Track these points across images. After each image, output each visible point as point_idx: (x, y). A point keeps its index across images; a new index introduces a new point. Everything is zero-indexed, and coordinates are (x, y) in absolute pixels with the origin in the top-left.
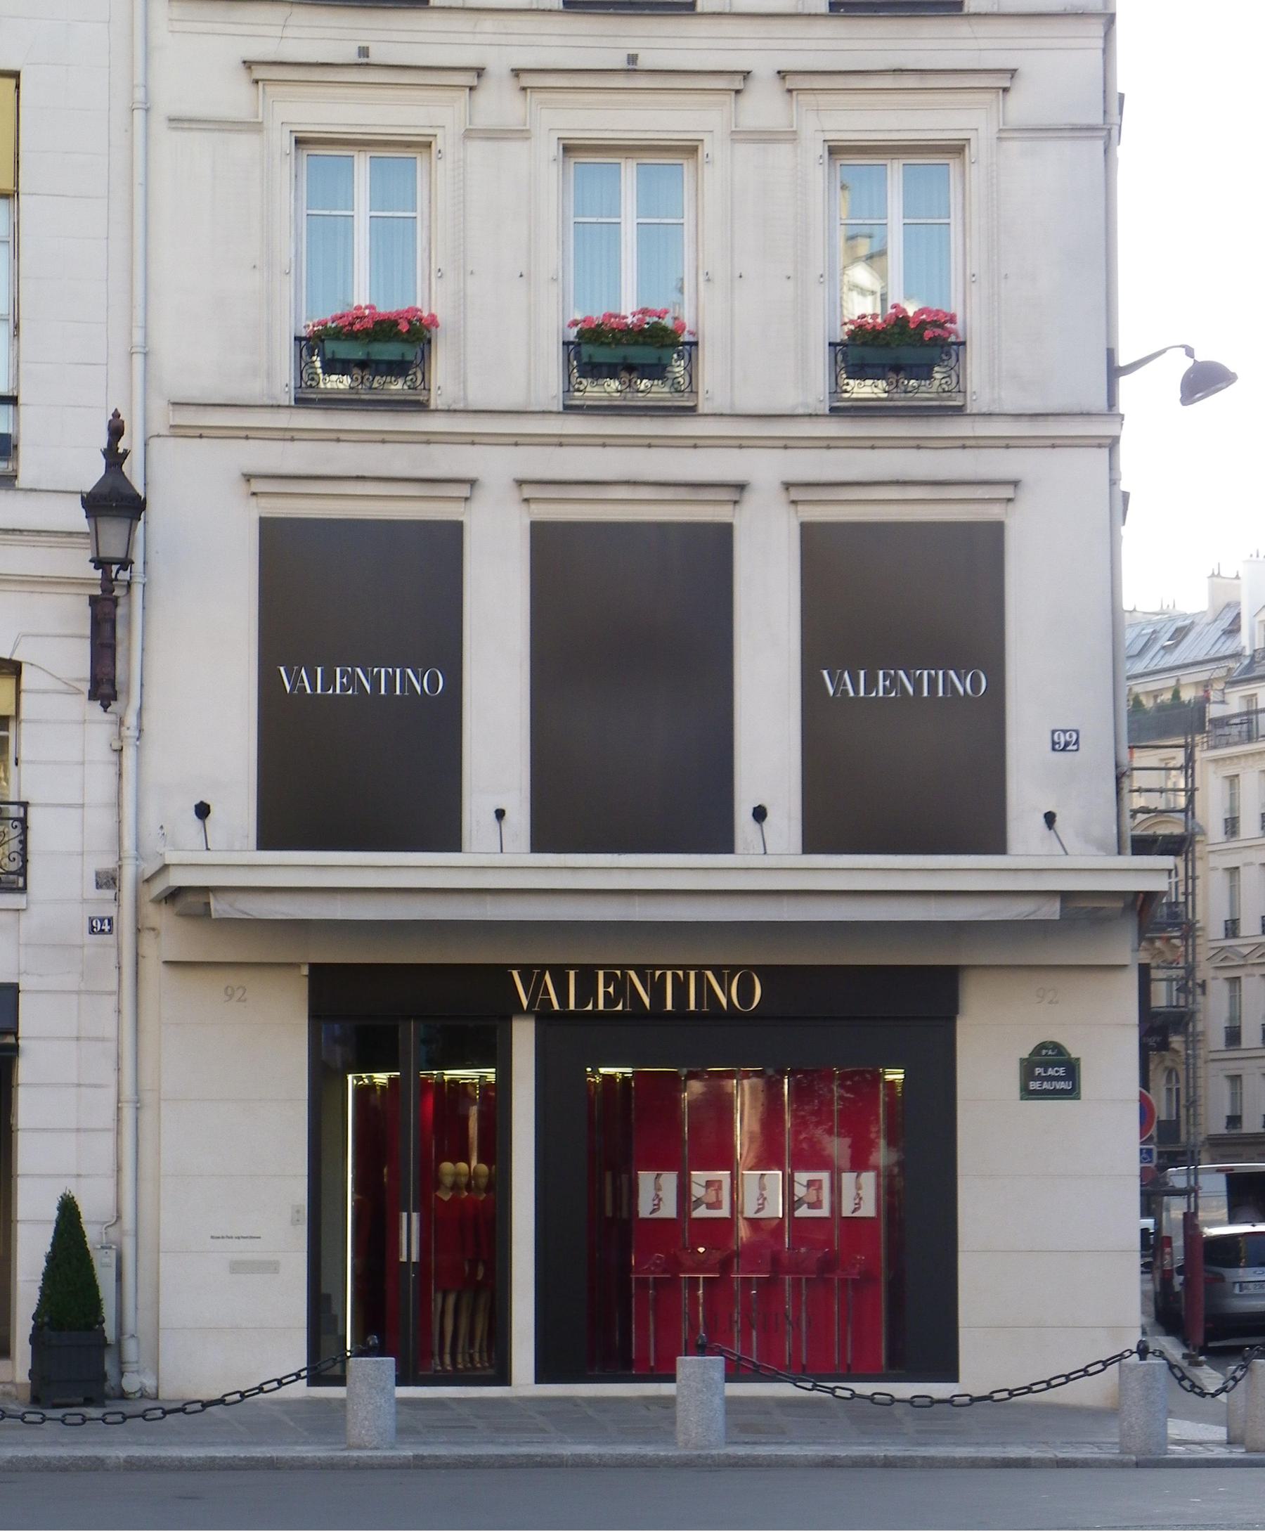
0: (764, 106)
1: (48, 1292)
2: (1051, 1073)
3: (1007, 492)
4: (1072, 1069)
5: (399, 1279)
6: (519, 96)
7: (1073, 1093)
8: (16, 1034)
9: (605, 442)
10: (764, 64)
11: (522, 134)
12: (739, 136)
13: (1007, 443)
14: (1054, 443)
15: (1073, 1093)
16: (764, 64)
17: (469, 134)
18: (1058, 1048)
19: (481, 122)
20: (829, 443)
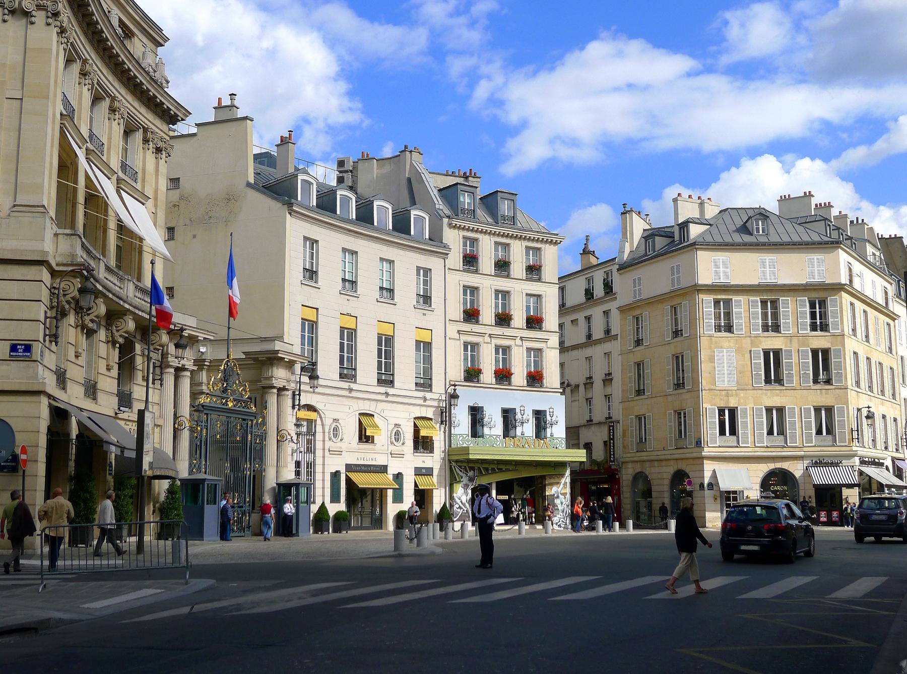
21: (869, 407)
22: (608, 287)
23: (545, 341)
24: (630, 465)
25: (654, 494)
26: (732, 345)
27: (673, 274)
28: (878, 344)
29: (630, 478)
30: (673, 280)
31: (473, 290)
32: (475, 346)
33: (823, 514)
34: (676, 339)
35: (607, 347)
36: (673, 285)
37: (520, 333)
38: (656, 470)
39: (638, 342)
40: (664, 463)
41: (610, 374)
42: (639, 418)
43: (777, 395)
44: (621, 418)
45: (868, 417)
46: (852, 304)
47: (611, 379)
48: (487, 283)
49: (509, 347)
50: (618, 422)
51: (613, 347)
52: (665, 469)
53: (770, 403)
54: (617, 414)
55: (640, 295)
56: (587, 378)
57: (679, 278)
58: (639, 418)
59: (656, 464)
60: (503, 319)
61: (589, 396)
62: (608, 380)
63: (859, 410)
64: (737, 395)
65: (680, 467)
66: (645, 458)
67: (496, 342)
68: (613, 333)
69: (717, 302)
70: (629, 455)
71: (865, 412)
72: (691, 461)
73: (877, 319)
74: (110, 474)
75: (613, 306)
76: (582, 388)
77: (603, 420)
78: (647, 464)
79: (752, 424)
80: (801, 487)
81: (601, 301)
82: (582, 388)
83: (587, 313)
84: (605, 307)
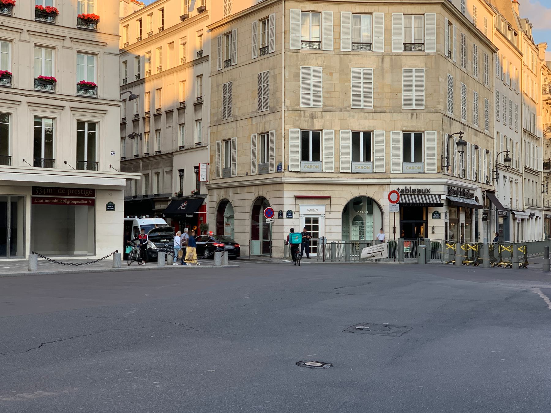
0: (68, 43)
1: (265, 201)
2: (111, 207)
3: (64, 38)
4: (114, 206)
5: (549, 169)
6: (28, 35)
7: (114, 210)
8: (342, 236)
9: (41, 97)
10: (68, 36)
11: (28, 42)
12: (64, 47)
13: (104, 104)
14: (111, 105)
15: (114, 210)
16: (68, 36)
17: (20, 41)
18: (112, 203)
19: (22, 39)
20: (77, 101)
21: (507, 152)
26: (320, 63)
28: (475, 72)
29: (215, 205)
38: (237, 197)
39: (228, 62)
40: (246, 189)
41: (201, 97)
42: (227, 141)
43: (365, 118)
45: (459, 144)
46: (463, 38)
52: (247, 196)
53: (356, 128)
56: (181, 103)
58: (227, 141)
59: (239, 190)
61: (182, 122)
62: (198, 104)
63: (450, 136)
64: (322, 117)
70: (214, 182)
71: (456, 138)
72: (271, 187)
73: (475, 48)
74: (201, 264)
76: (176, 113)
78: (231, 191)
79: (337, 148)
81: (195, 21)
82: (176, 113)
83: (183, 34)
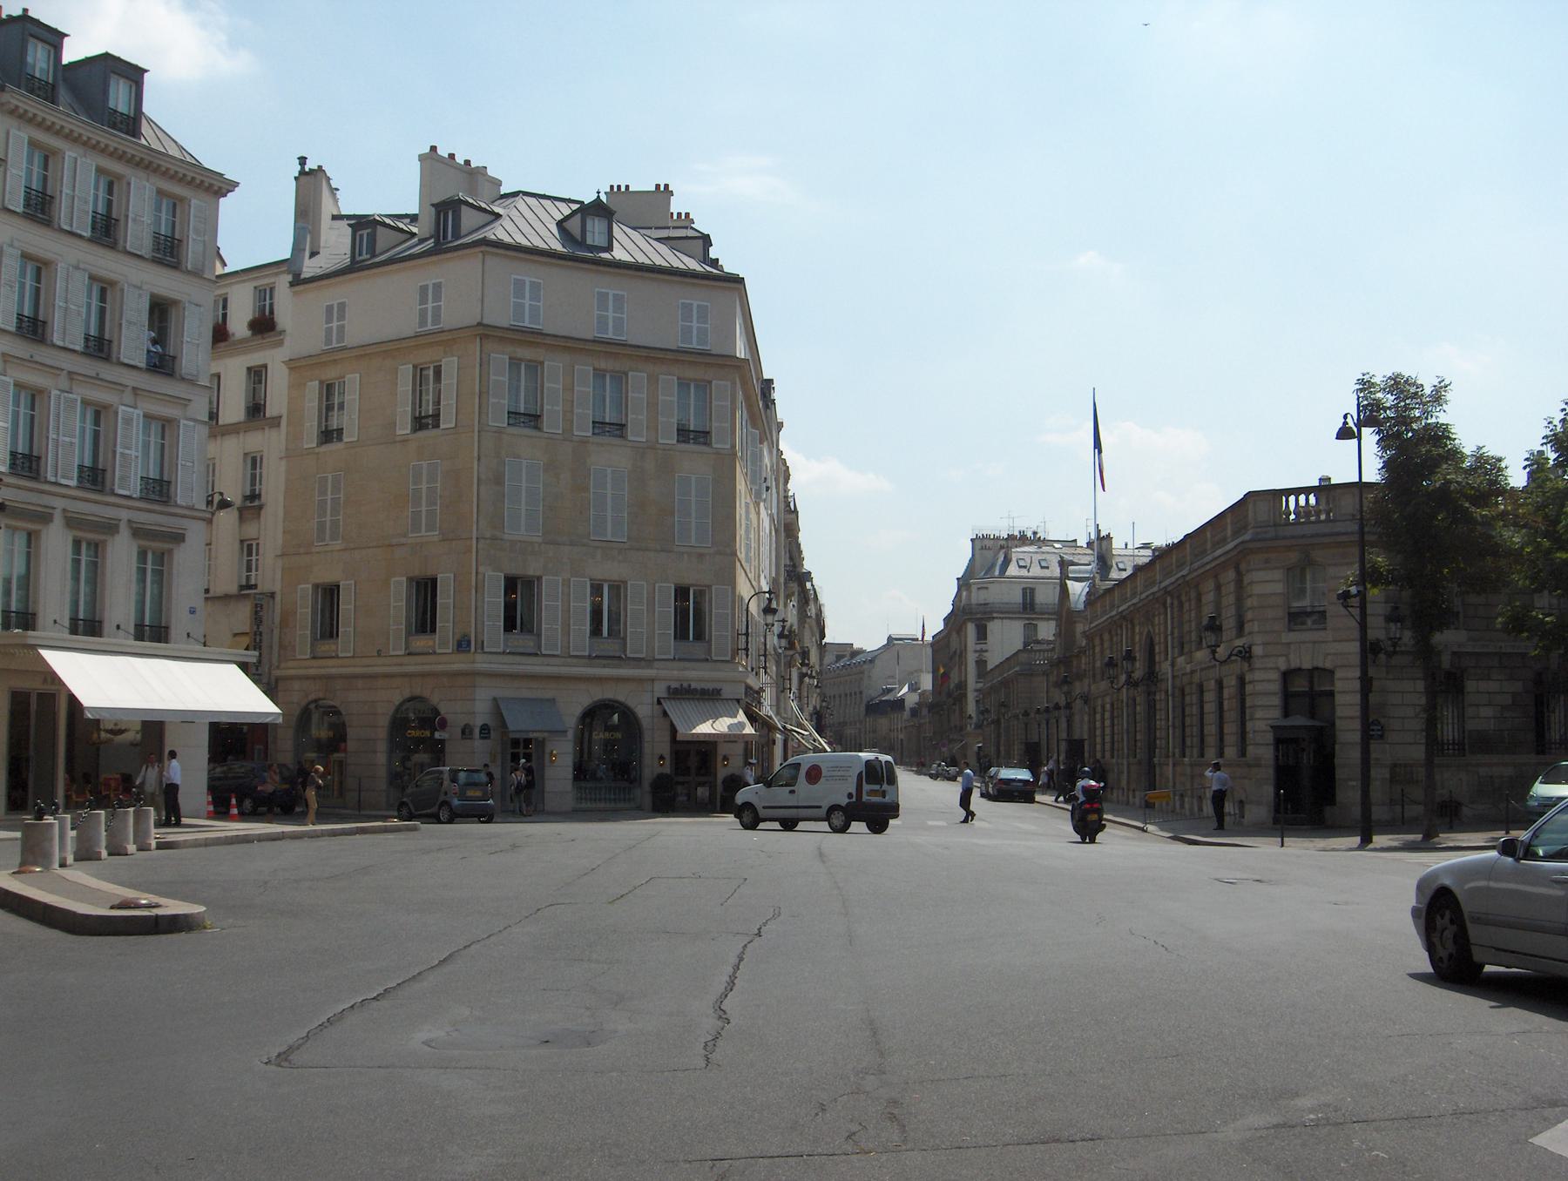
22: (264, 325)
23: (185, 403)
24: (296, 685)
25: (351, 745)
27: (423, 300)
30: (329, 331)
31: (40, 267)
32: (35, 396)
33: (1420, 809)
34: (420, 434)
35: (255, 441)
36: (423, 322)
37: (131, 379)
44: (277, 588)
47: (260, 507)
48: (75, 261)
49: (106, 407)
50: (272, 595)
51: (270, 443)
54: (269, 576)
55: (341, 338)
57: (437, 310)
60: (99, 347)
65: (417, 692)
66: (334, 671)
67: (81, 392)
68: (271, 411)
69: (515, 363)
75: (275, 359)
77: (233, 589)
80: (647, 737)
81: (242, 346)
84: (255, 359)
